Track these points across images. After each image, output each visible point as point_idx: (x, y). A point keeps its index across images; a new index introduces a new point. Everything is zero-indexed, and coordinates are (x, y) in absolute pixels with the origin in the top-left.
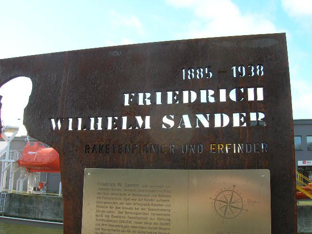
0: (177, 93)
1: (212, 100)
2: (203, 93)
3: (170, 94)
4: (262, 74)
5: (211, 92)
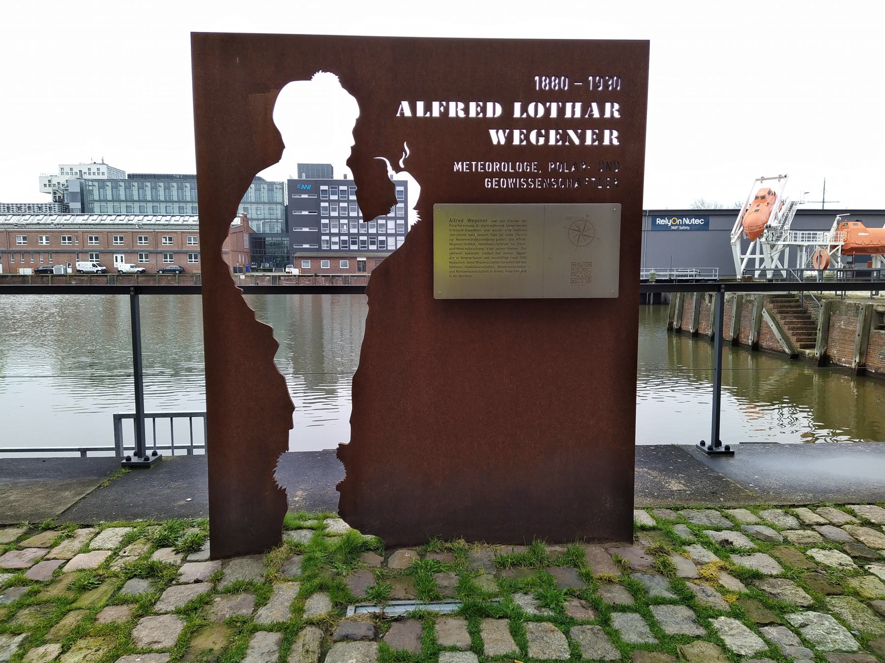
0: (543, 131)
1: (462, 114)
2: (452, 105)
3: (473, 105)
4: (566, 88)
5: (461, 105)
